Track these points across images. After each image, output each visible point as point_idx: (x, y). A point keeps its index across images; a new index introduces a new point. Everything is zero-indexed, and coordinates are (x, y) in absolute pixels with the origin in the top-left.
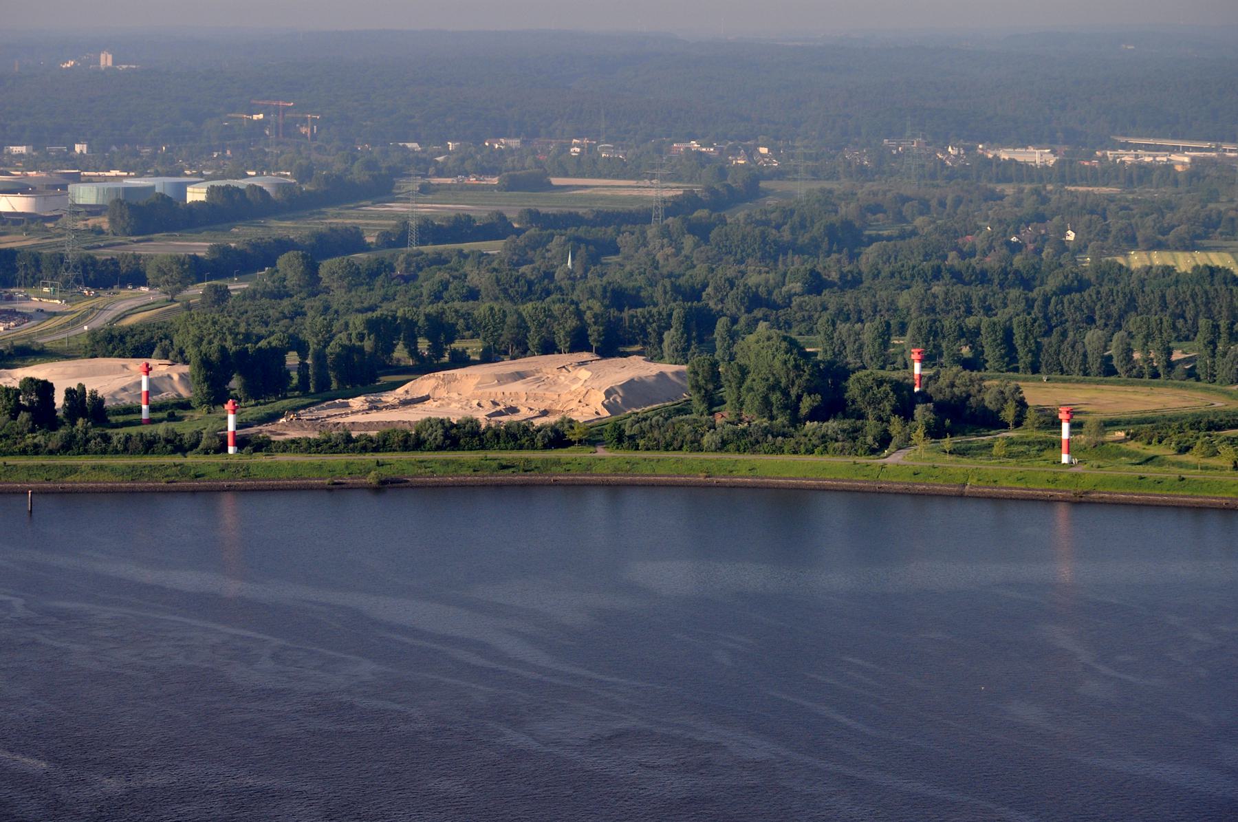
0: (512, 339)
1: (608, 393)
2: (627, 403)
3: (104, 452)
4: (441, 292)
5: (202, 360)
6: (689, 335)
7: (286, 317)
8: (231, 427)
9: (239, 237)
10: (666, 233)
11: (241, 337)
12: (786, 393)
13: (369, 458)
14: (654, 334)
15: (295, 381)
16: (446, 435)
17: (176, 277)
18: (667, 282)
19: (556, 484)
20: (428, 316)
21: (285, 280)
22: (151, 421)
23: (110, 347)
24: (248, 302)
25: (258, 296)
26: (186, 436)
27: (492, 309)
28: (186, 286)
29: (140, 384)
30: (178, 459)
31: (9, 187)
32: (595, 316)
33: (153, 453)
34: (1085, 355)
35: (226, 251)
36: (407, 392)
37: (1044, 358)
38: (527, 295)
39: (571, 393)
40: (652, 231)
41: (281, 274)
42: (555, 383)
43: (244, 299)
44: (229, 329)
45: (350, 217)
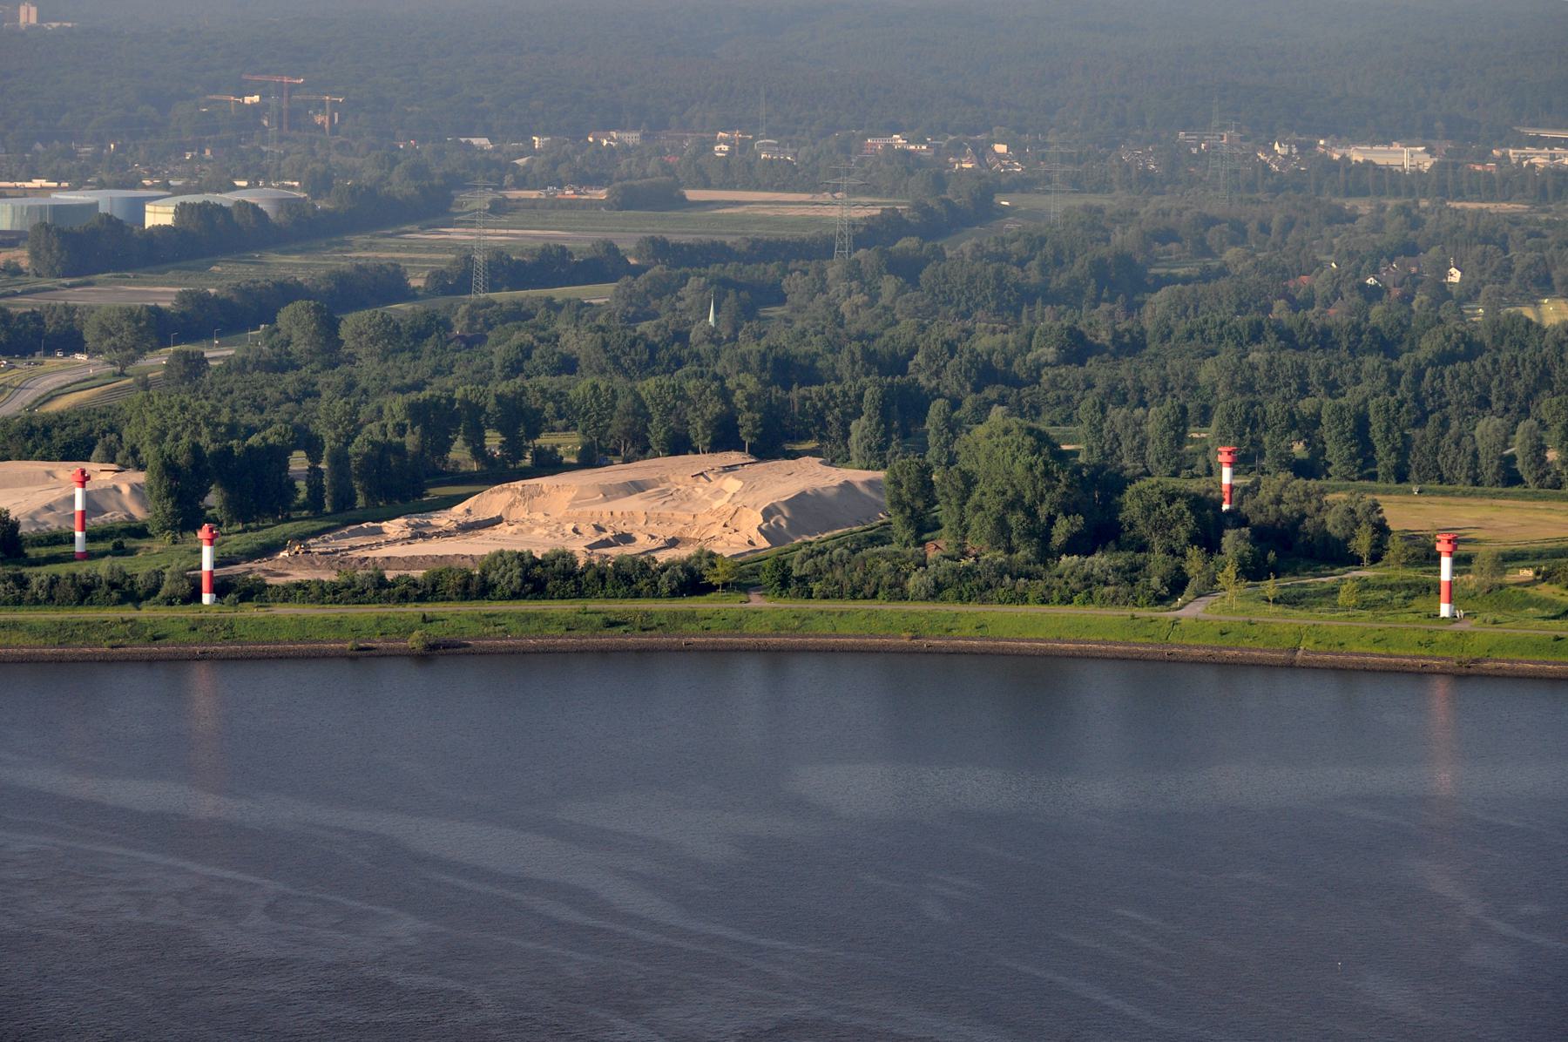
0: (625, 433)
1: (767, 513)
2: (796, 527)
3: (18, 602)
4: (520, 362)
5: (164, 464)
7: (289, 399)
8: (207, 565)
9: (221, 278)
10: (854, 272)
11: (222, 429)
12: (1031, 513)
13: (412, 610)
14: (836, 425)
15: (302, 496)
16: (526, 578)
18: (856, 346)
19: (688, 649)
21: (289, 343)
22: (88, 556)
23: (30, 444)
25: (249, 367)
26: (140, 578)
27: (595, 387)
28: (142, 353)
29: (72, 499)
30: (128, 612)
32: (749, 398)
33: (91, 603)
34: (1475, 455)
35: (202, 300)
36: (468, 511)
37: (1414, 459)
38: (648, 365)
39: (712, 513)
40: (834, 269)
41: (283, 335)
42: (689, 498)
43: (229, 371)
44: (206, 419)
45: (386, 249)
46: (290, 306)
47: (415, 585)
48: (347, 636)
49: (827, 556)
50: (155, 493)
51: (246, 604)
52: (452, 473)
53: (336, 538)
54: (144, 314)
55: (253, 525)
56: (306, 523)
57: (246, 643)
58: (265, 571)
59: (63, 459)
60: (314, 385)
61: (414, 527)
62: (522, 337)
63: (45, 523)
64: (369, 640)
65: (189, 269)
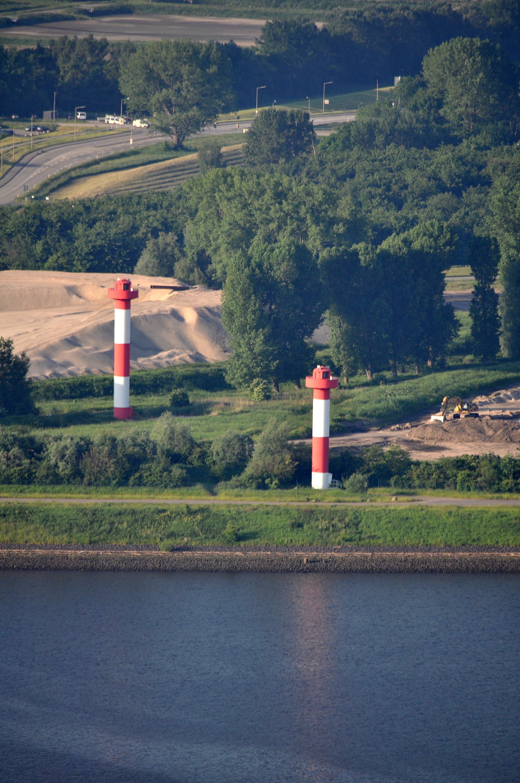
3: (27, 479)
5: (251, 277)
7: (442, 188)
8: (319, 428)
11: (340, 228)
15: (464, 332)
17: (189, 92)
21: (440, 104)
22: (132, 414)
23: (39, 247)
24: (355, 152)
25: (379, 139)
26: (216, 447)
28: (210, 115)
29: (108, 329)
30: (196, 497)
33: (140, 483)
41: (431, 91)
43: (347, 145)
44: (314, 211)
46: (444, 46)
50: (237, 323)
51: (380, 490)
54: (214, 54)
55: (388, 375)
56: (471, 373)
57: (379, 548)
58: (407, 442)
59: (91, 270)
60: (480, 168)
63: (66, 365)
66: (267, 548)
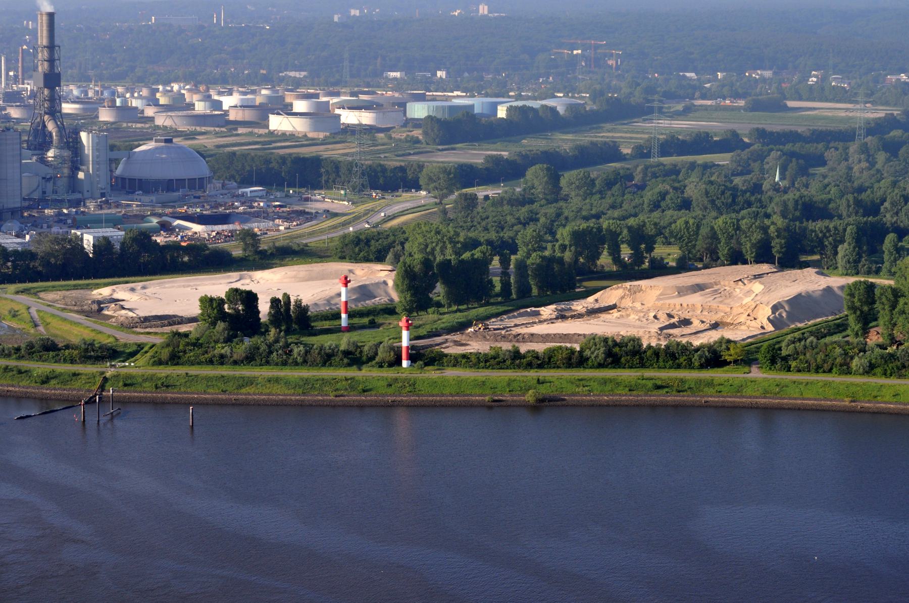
0: (707, 249)
1: (775, 308)
2: (792, 317)
3: (285, 364)
4: (659, 202)
5: (406, 271)
6: (860, 248)
7: (520, 223)
8: (405, 342)
9: (532, 144)
10: (864, 149)
11: (459, 245)
13: (533, 374)
14: (830, 247)
16: (609, 353)
18: (850, 197)
19: (707, 406)
20: (630, 229)
22: (350, 328)
26: (366, 348)
27: (687, 223)
29: (339, 295)
31: (355, 105)
32: (778, 230)
33: (331, 365)
35: (498, 160)
36: (597, 300)
38: (731, 205)
39: (742, 306)
40: (853, 148)
42: (730, 295)
45: (620, 131)
46: (533, 167)
47: (537, 358)
48: (488, 392)
49: (803, 343)
50: (401, 288)
51: (430, 368)
52: (597, 272)
53: (509, 318)
54: (453, 170)
55: (465, 307)
57: (423, 395)
60: (537, 214)
61: (560, 311)
62: (663, 186)
64: (501, 395)
65: (510, 141)
66: (376, 395)
